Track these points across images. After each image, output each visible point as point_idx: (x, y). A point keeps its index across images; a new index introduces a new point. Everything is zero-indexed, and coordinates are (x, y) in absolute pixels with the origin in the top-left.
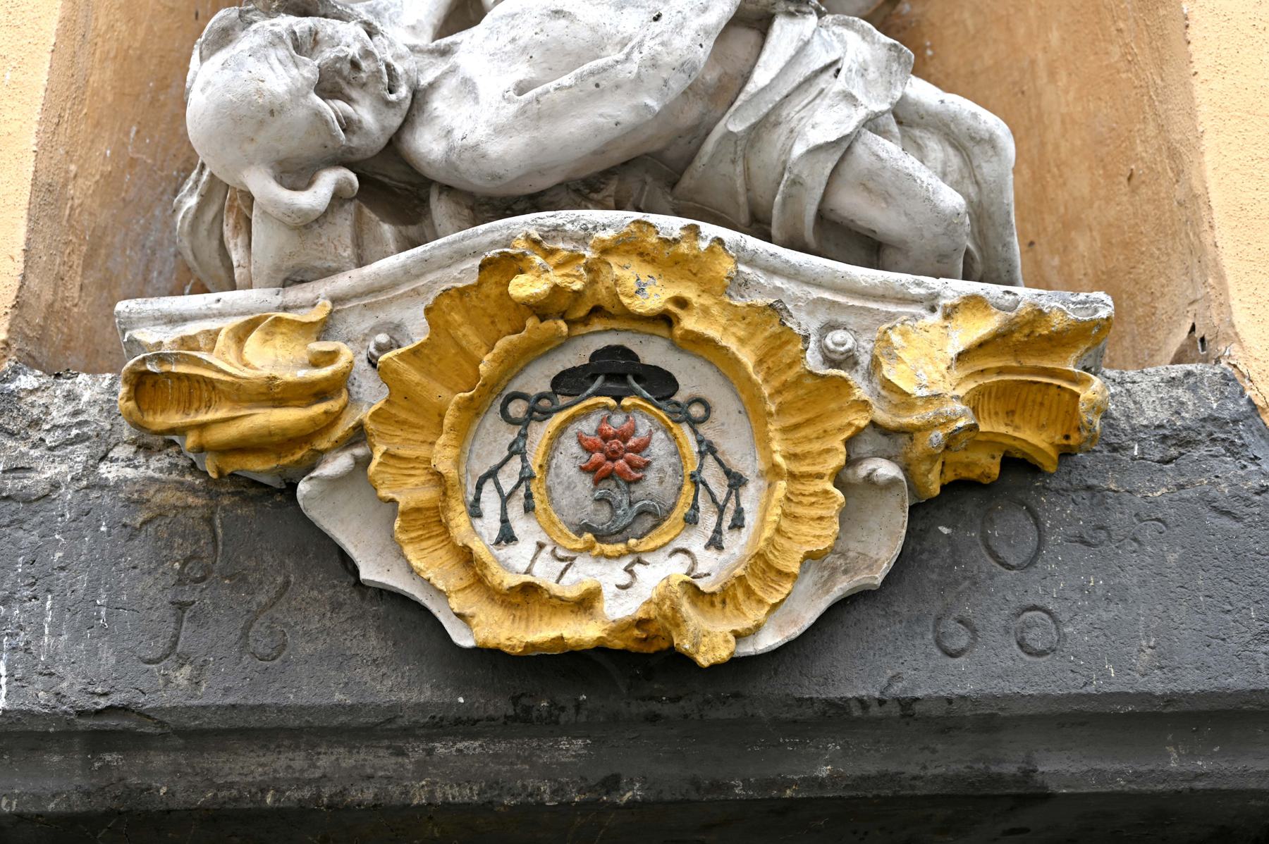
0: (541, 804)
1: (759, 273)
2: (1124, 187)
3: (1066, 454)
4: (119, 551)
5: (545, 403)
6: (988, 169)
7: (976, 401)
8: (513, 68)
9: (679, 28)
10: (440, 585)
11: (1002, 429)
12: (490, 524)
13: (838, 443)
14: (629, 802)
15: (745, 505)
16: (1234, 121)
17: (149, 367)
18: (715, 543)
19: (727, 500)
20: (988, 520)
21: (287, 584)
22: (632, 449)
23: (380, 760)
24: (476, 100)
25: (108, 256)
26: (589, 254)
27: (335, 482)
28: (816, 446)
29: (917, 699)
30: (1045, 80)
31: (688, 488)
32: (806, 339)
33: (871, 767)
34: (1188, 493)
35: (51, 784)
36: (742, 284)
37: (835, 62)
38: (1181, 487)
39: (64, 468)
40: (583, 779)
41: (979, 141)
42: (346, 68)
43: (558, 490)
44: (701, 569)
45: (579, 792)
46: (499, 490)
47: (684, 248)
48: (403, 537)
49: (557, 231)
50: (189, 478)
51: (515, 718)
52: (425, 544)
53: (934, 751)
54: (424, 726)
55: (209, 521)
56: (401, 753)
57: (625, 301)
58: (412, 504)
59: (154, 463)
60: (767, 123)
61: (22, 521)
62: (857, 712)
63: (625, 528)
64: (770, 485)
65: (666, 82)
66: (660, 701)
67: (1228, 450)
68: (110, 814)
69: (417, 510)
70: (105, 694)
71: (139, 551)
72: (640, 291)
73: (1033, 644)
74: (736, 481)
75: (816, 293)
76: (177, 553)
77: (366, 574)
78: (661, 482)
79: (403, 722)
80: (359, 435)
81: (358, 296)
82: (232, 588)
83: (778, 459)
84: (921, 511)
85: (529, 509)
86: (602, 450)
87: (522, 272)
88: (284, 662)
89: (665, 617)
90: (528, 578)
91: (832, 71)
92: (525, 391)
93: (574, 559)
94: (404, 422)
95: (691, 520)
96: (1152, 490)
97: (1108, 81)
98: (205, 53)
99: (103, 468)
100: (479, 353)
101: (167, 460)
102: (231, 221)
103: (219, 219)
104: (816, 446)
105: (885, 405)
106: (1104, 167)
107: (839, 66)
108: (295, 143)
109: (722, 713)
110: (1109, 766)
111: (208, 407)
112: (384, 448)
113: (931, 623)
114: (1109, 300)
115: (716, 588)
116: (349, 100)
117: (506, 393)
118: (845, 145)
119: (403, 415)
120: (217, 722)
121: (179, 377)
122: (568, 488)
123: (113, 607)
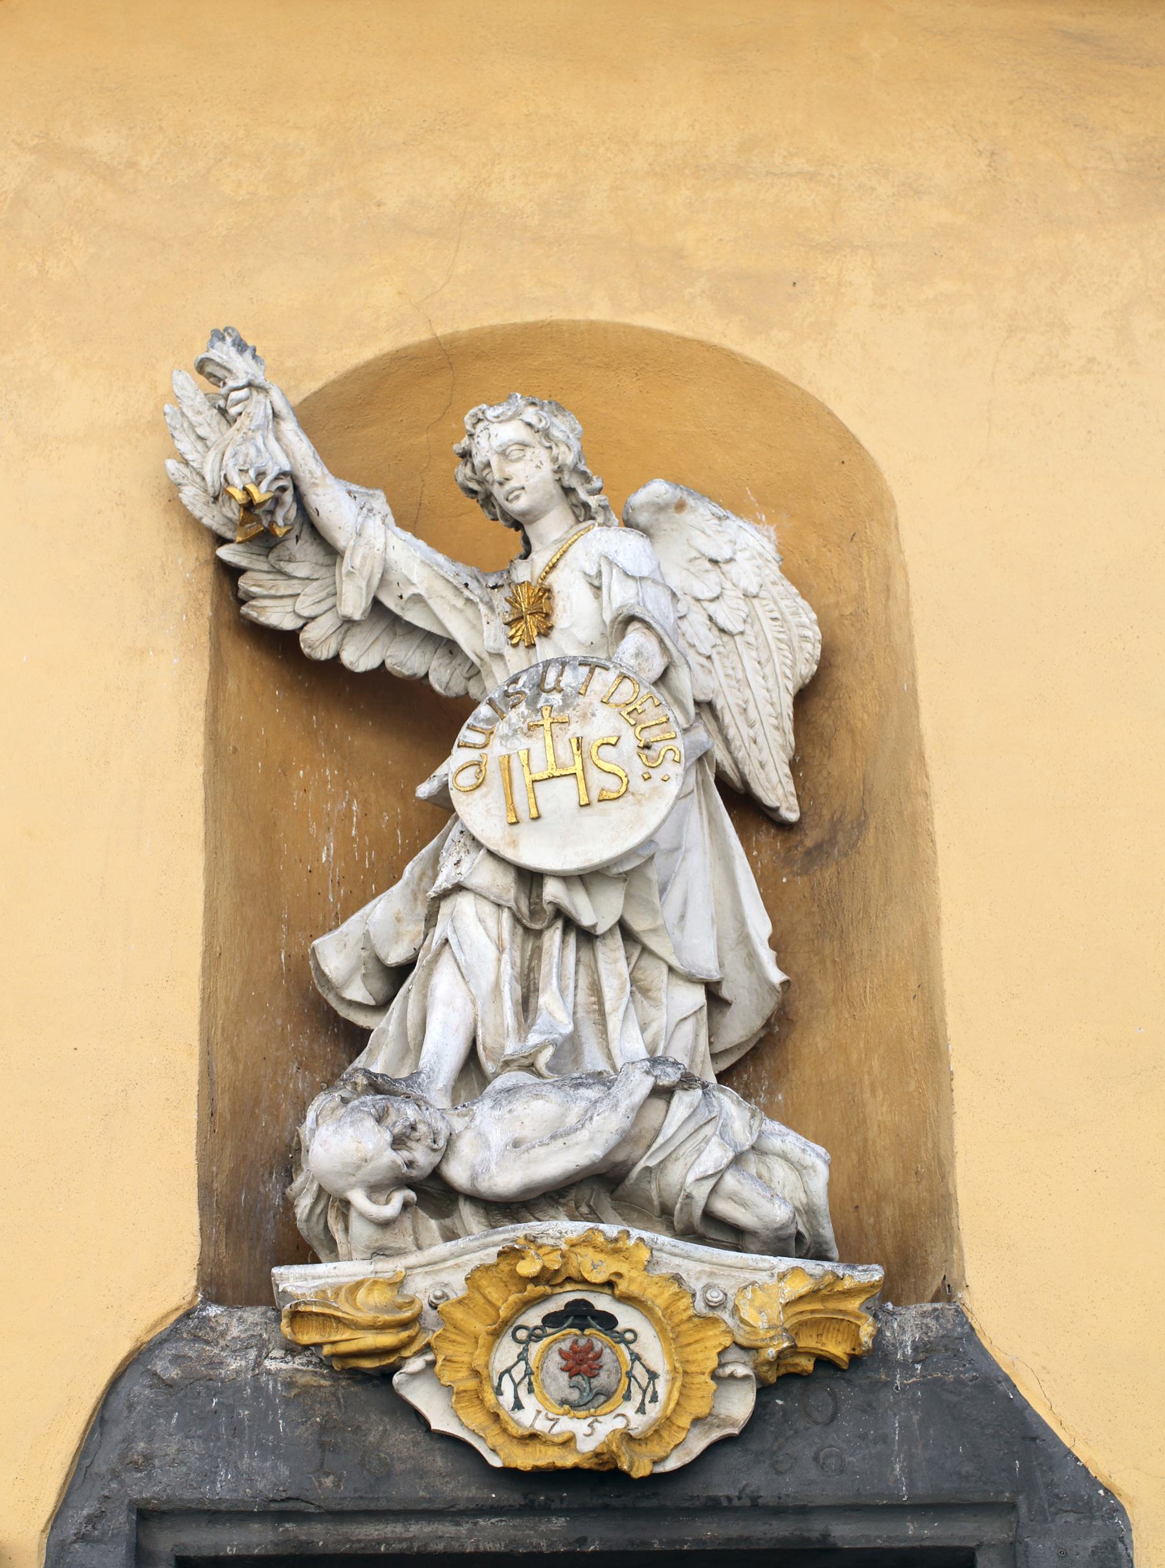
5: (538, 1332)
12: (507, 1399)
14: (592, 1551)
15: (657, 1389)
19: (648, 1386)
21: (385, 1431)
27: (414, 1375)
31: (625, 1380)
35: (255, 1539)
43: (548, 1381)
45: (563, 1546)
46: (513, 1380)
53: (771, 1525)
56: (458, 1524)
59: (297, 1360)
62: (725, 1503)
63: (588, 1403)
77: (434, 1426)
80: (428, 1348)
84: (764, 1391)
85: (531, 1390)
87: (523, 1258)
94: (454, 1341)
95: (627, 1397)
101: (305, 1359)
102: (333, 1215)
103: (324, 1212)
117: (515, 1325)
118: (719, 1175)
119: (453, 1337)
122: (554, 1380)
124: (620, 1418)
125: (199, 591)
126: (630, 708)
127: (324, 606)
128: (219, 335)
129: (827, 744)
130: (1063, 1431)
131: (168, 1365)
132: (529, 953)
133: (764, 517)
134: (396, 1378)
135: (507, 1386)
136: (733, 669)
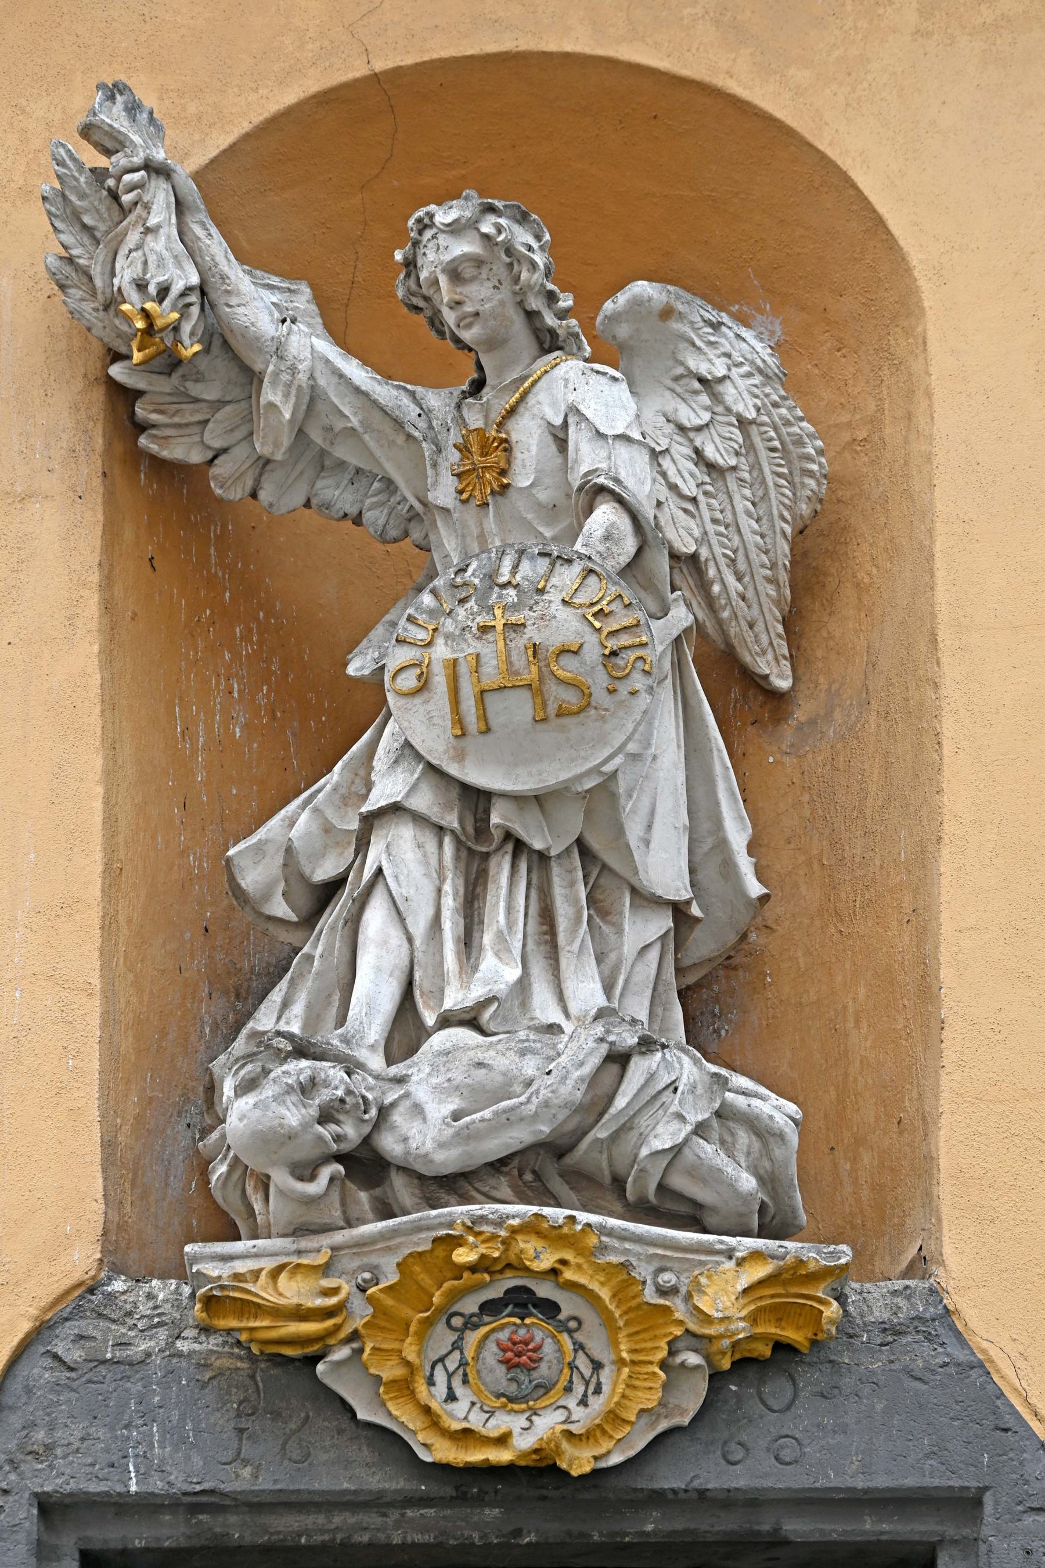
0: (473, 1544)
1: (615, 1241)
2: (895, 1128)
3: (814, 1343)
4: (197, 1397)
5: (475, 1319)
6: (778, 1153)
7: (753, 1318)
8: (450, 1099)
9: (564, 1078)
10: (411, 1426)
11: (773, 1330)
13: (663, 1344)
15: (602, 1380)
16: (965, 1105)
17: (215, 1293)
18: (583, 1402)
19: (591, 1377)
20: (762, 1382)
21: (307, 1417)
22: (529, 1350)
23: (372, 1519)
24: (425, 1120)
25: (143, 1175)
26: (503, 1233)
27: (339, 1364)
28: (649, 1345)
29: (708, 1490)
30: (852, 1025)
32: (644, 1283)
33: (679, 1525)
34: (896, 1366)
35: (166, 1532)
36: (603, 1248)
37: (674, 1082)
38: (891, 1362)
39: (152, 1343)
40: (499, 1530)
41: (774, 1135)
42: (337, 1104)
43: (484, 1373)
44: (574, 1418)
45: (497, 1537)
46: (446, 1370)
47: (565, 1230)
48: (385, 1397)
49: (483, 1219)
50: (236, 1350)
51: (457, 1498)
52: (399, 1401)
53: (719, 1517)
54: (400, 1501)
55: (252, 1377)
56: (385, 1515)
57: (528, 1263)
58: (391, 1378)
60: (626, 1127)
61: (129, 1377)
64: (618, 1369)
65: (554, 1116)
66: (547, 1488)
67: (926, 1338)
68: (202, 1548)
69: (394, 1381)
70: (199, 1483)
71: (209, 1396)
72: (537, 1257)
73: (784, 1458)
74: (597, 1366)
75: (652, 1250)
76: (234, 1398)
77: (360, 1416)
78: (550, 1368)
79: (385, 1500)
80: (355, 1336)
81: (349, 1247)
82: (273, 1420)
83: (624, 1355)
84: (716, 1378)
85: (465, 1381)
86: (512, 1351)
87: (460, 1246)
88: (310, 1464)
89: (551, 1450)
90: (465, 1425)
91: (672, 1088)
92: (461, 1311)
93: (493, 1412)
94: (384, 1328)
95: (568, 1389)
96: (872, 1363)
97: (893, 1042)
98: (239, 1092)
99: (179, 1344)
100: (433, 1290)
101: (221, 1339)
102: (252, 1183)
104: (649, 1345)
105: (695, 1320)
106: (885, 1106)
107: (677, 1084)
108: (304, 1152)
109: (587, 1496)
110: (827, 1527)
111: (256, 1318)
112: (372, 1345)
113: (720, 1445)
114: (849, 1252)
115: (582, 1431)
116: (337, 1122)
118: (676, 1149)
119: (383, 1324)
120: (269, 1499)
121: (235, 1299)
123: (197, 1431)
124: (561, 1410)
125: (89, 418)
126: (596, 608)
127: (239, 435)
128: (113, 91)
129: (829, 598)
130: (1038, 1423)
131: (71, 1346)
132: (474, 876)
133: (768, 306)
134: (320, 1367)
135: (440, 1376)
136: (722, 512)
